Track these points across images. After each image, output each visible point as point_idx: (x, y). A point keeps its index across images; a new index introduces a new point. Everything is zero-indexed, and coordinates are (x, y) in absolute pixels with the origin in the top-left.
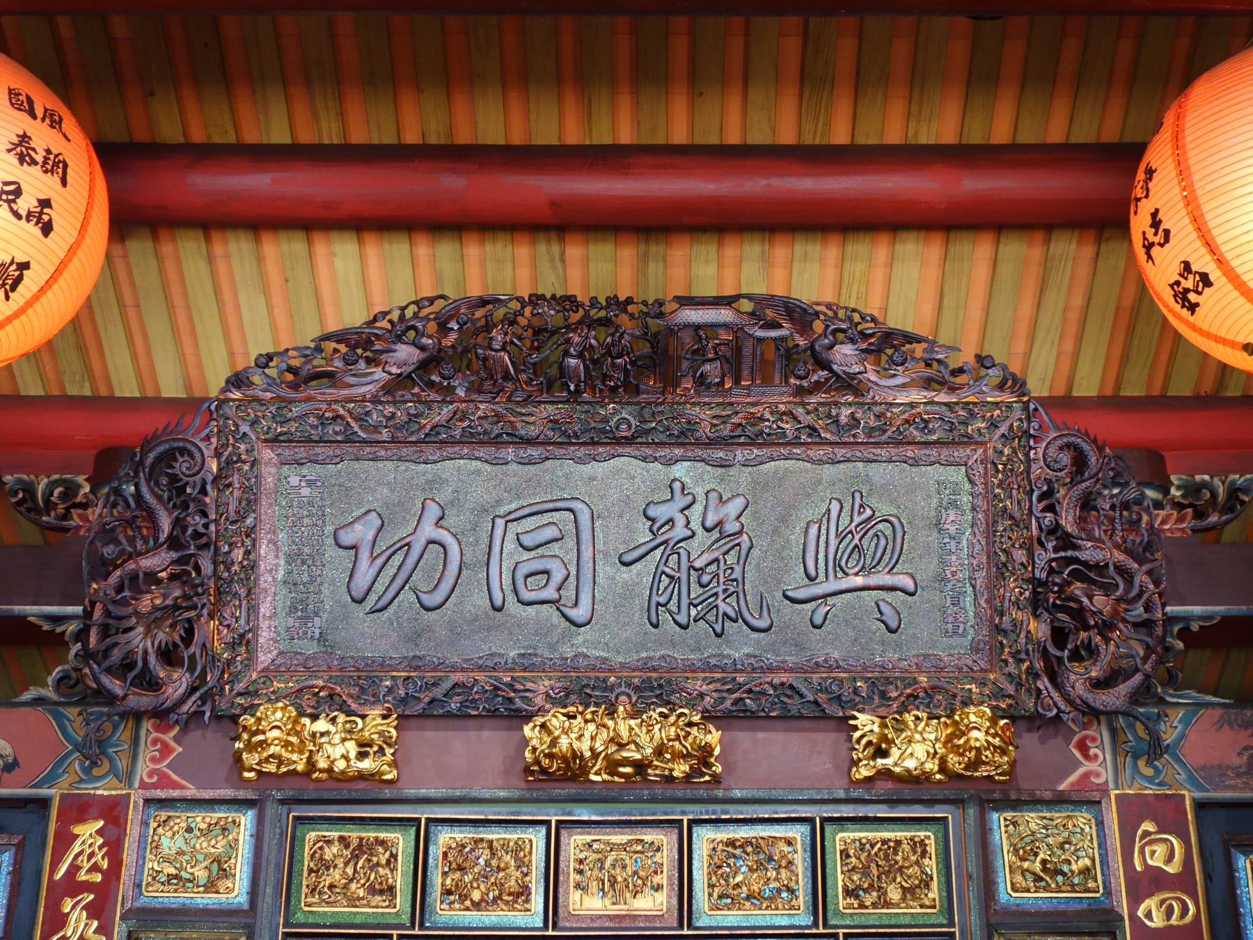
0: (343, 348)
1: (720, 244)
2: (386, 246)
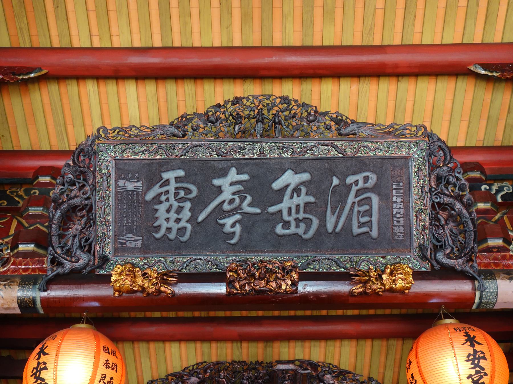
0: (175, 378)
1: (289, 342)
2: (188, 344)
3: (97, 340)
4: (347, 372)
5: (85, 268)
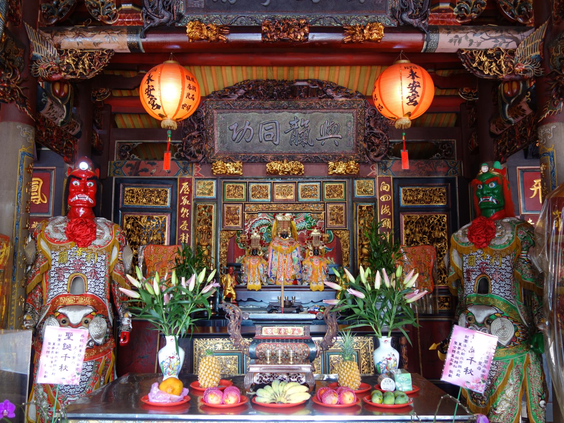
3: (182, 72)
4: (342, 88)
5: (168, 22)
